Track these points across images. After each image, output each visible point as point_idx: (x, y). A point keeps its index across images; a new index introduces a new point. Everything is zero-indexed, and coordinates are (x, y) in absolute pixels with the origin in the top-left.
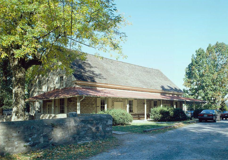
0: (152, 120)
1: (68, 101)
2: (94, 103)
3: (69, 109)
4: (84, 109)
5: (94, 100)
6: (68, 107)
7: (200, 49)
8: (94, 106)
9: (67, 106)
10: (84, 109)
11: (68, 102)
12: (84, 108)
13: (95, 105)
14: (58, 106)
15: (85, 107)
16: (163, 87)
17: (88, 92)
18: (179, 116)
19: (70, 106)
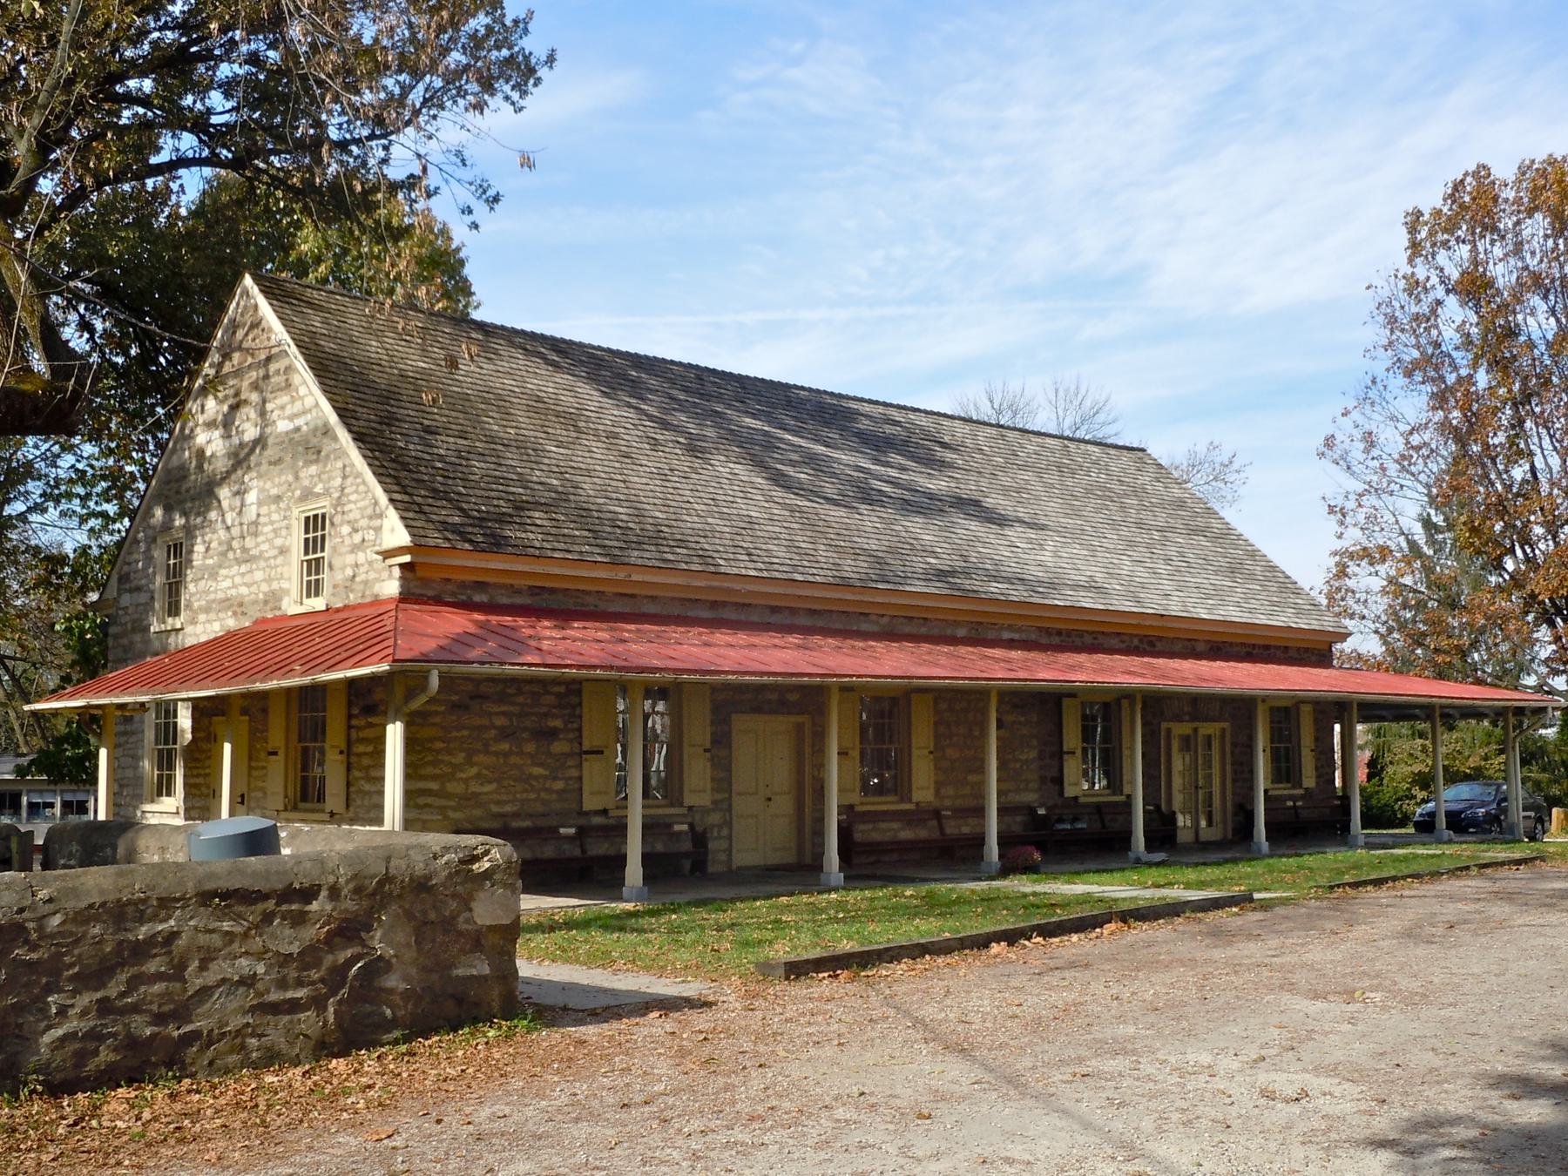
0: (1542, 1053)
1: (356, 711)
2: (558, 723)
3: (356, 774)
4: (474, 771)
5: (558, 695)
6: (353, 759)
7: (1551, 155)
8: (559, 747)
9: (343, 746)
10: (474, 771)
11: (350, 716)
12: (472, 765)
13: (571, 741)
14: (282, 744)
15: (480, 758)
16: (482, 113)
17: (658, 771)
18: (1406, 620)
19: (360, 748)
